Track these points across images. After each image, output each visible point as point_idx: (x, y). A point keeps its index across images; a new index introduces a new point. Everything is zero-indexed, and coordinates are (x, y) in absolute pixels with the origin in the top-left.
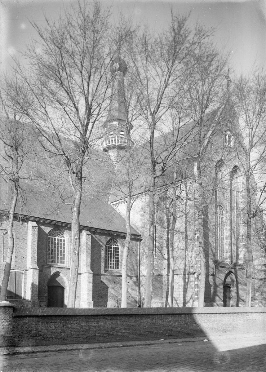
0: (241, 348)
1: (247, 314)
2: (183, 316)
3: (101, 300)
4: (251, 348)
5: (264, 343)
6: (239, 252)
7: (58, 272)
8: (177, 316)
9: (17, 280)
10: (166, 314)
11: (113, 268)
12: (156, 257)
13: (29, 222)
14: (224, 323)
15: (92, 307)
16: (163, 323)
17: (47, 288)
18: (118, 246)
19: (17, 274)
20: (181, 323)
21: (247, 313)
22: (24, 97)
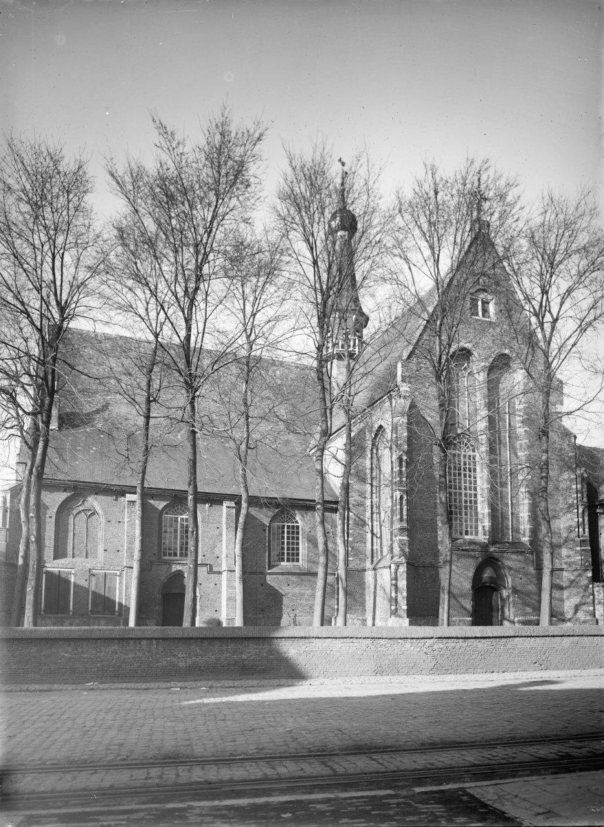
0: (598, 687)
1: (307, 641)
2: (144, 642)
3: (260, 616)
4: (591, 690)
5: (599, 691)
6: (60, 477)
7: (180, 571)
8: (132, 642)
9: (107, 586)
10: (107, 639)
11: (288, 560)
12: (350, 539)
13: (127, 495)
14: (244, 657)
15: (238, 622)
16: (98, 654)
17: (159, 596)
18: (297, 522)
19: (108, 577)
20: (139, 654)
21: (309, 638)
22: (232, 232)
